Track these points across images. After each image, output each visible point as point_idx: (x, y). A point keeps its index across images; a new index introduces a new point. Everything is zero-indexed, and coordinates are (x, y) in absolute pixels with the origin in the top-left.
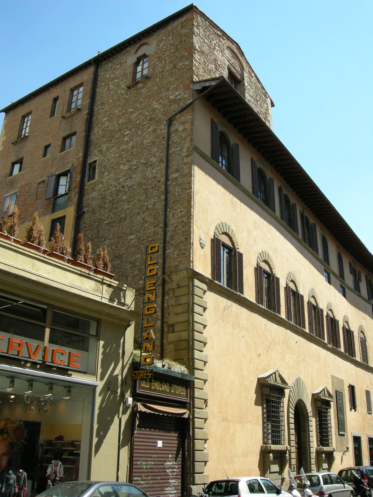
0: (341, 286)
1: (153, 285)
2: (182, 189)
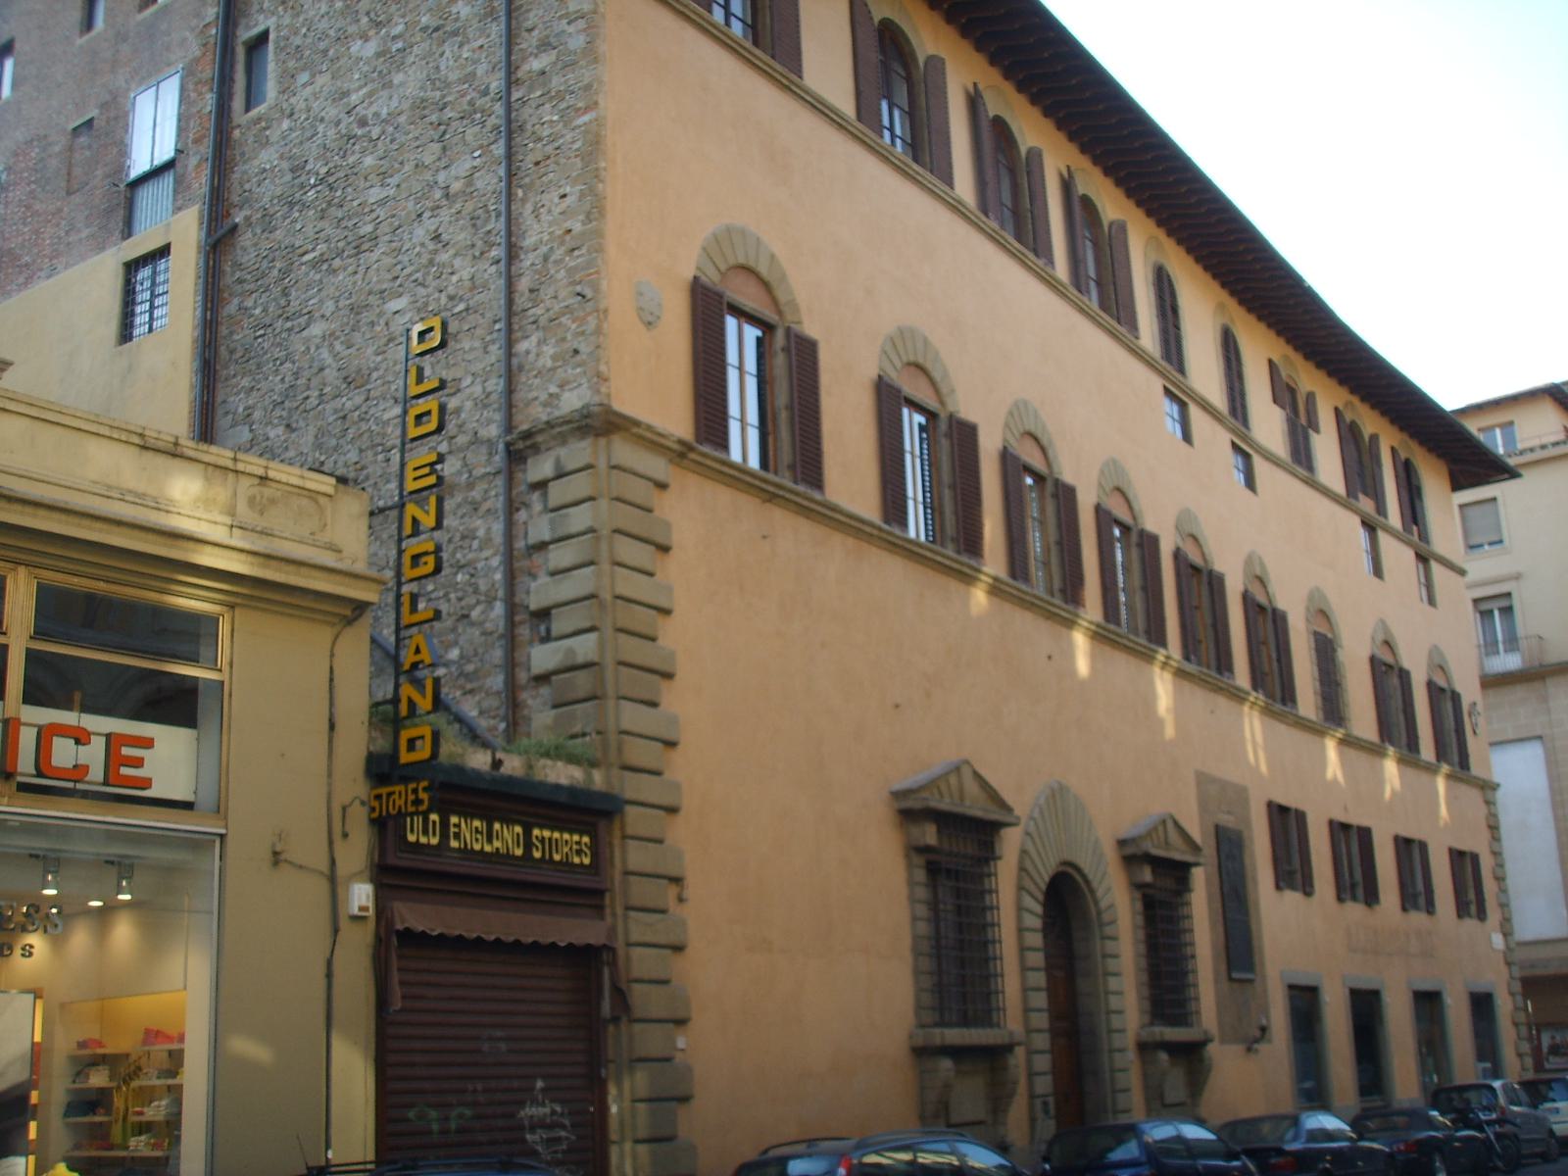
0: (1235, 447)
1: (427, 470)
2: (563, 114)
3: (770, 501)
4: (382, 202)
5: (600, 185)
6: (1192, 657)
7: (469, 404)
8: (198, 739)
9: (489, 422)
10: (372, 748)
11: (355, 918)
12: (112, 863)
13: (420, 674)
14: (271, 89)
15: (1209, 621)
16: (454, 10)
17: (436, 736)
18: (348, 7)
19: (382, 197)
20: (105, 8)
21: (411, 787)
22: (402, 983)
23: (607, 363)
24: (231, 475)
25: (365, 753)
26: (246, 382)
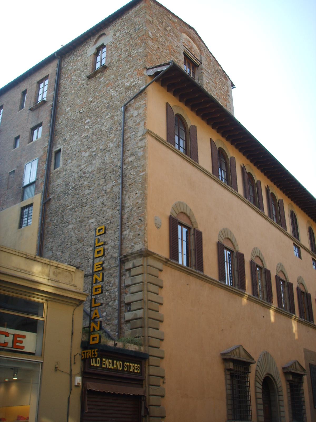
1: (100, 266)
3: (189, 275)
4: (89, 194)
5: (146, 191)
6: (302, 317)
7: (110, 248)
8: (37, 336)
9: (116, 252)
10: (82, 340)
11: (76, 386)
12: (12, 369)
13: (96, 320)
14: (61, 164)
15: (307, 307)
16: (109, 145)
17: (100, 337)
18: (81, 143)
19: (89, 192)
20: (20, 142)
21: (92, 348)
22: (88, 405)
23: (147, 238)
24: (49, 266)
25: (80, 341)
26: (51, 240)
